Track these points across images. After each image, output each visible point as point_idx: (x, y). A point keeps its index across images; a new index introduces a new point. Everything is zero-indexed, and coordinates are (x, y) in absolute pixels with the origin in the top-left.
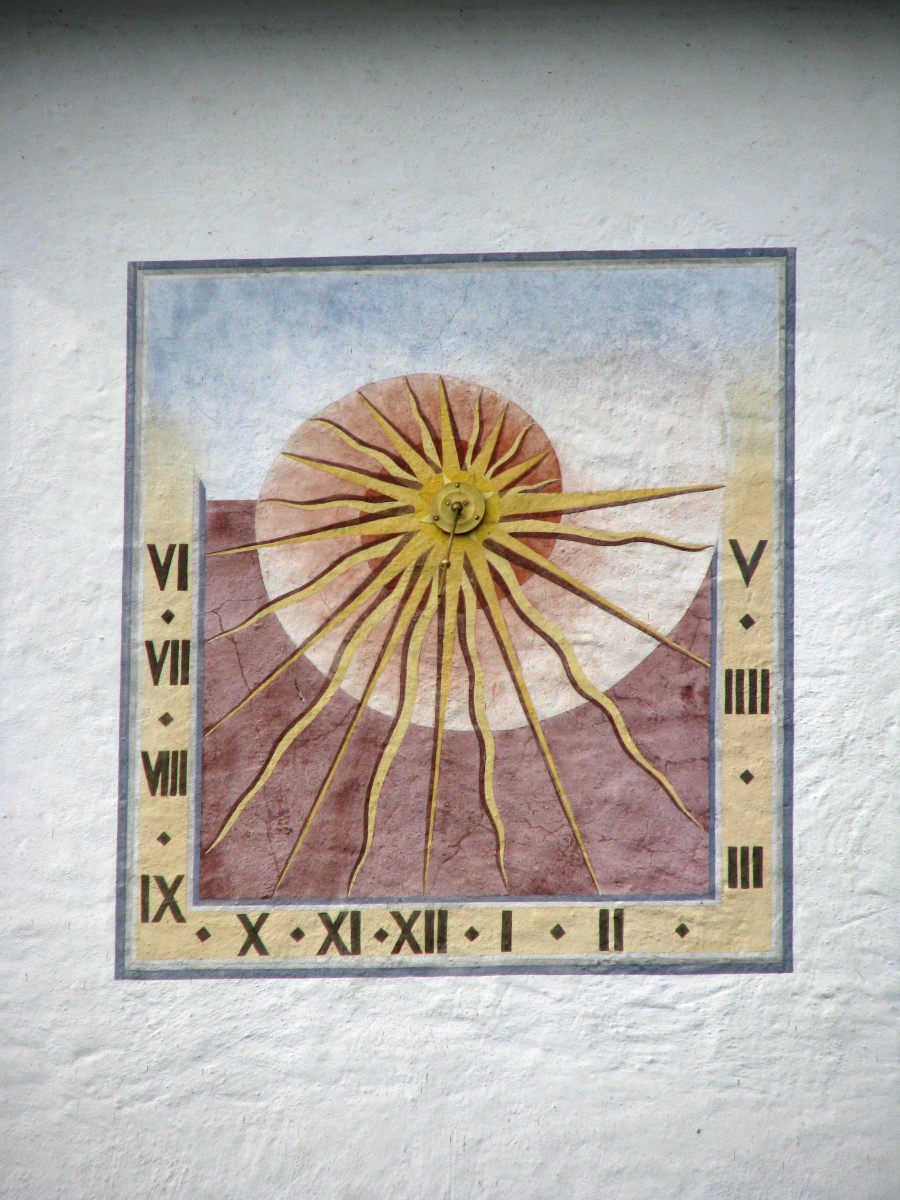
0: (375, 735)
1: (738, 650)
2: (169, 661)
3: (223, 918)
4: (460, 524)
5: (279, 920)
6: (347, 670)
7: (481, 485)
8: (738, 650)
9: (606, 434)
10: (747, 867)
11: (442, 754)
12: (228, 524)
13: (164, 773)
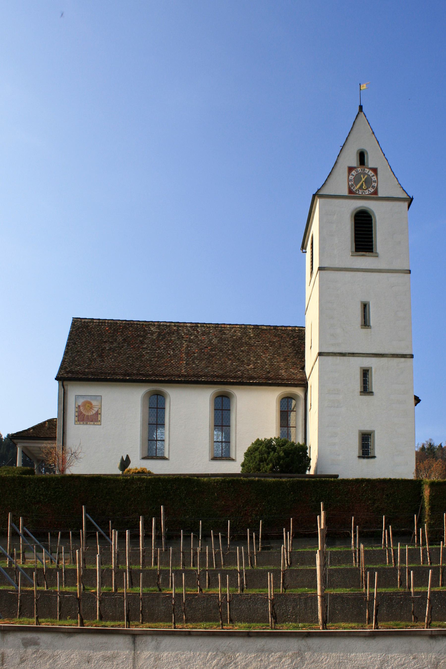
0: (85, 415)
1: (99, 412)
2: (77, 412)
3: (79, 422)
4: (88, 406)
5: (81, 422)
6: (84, 412)
7: (89, 405)
8: (99, 412)
9: (94, 403)
10: (99, 421)
11: (88, 416)
12: (79, 406)
13: (76, 416)
